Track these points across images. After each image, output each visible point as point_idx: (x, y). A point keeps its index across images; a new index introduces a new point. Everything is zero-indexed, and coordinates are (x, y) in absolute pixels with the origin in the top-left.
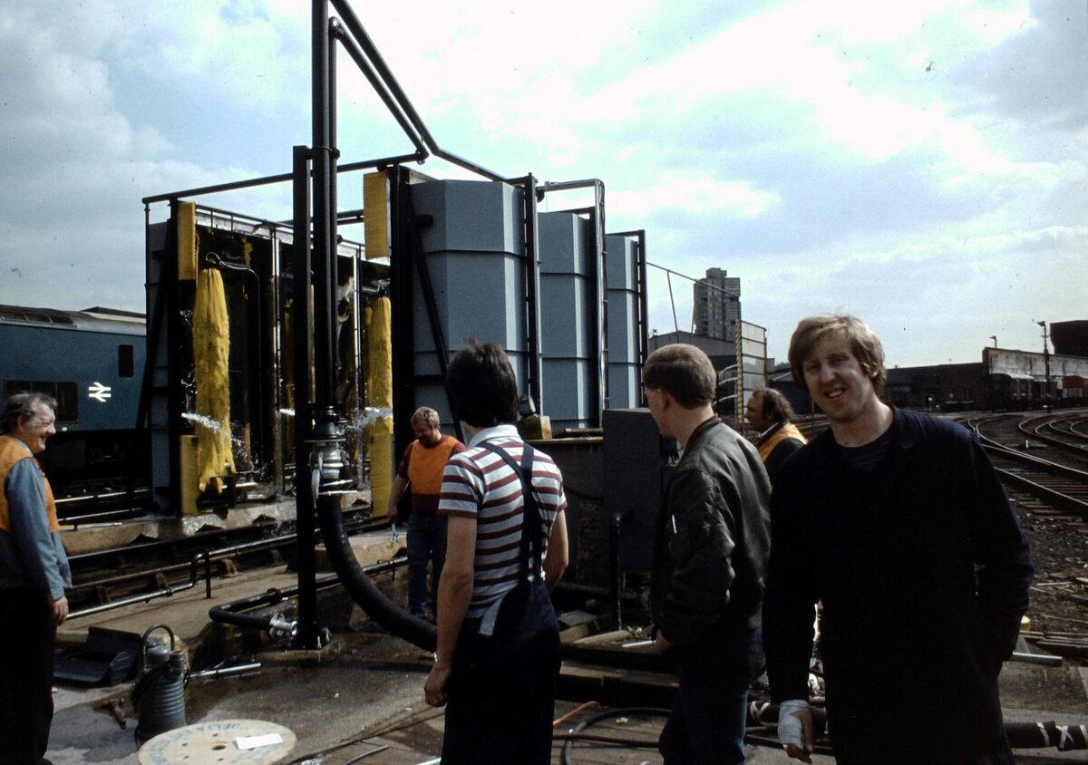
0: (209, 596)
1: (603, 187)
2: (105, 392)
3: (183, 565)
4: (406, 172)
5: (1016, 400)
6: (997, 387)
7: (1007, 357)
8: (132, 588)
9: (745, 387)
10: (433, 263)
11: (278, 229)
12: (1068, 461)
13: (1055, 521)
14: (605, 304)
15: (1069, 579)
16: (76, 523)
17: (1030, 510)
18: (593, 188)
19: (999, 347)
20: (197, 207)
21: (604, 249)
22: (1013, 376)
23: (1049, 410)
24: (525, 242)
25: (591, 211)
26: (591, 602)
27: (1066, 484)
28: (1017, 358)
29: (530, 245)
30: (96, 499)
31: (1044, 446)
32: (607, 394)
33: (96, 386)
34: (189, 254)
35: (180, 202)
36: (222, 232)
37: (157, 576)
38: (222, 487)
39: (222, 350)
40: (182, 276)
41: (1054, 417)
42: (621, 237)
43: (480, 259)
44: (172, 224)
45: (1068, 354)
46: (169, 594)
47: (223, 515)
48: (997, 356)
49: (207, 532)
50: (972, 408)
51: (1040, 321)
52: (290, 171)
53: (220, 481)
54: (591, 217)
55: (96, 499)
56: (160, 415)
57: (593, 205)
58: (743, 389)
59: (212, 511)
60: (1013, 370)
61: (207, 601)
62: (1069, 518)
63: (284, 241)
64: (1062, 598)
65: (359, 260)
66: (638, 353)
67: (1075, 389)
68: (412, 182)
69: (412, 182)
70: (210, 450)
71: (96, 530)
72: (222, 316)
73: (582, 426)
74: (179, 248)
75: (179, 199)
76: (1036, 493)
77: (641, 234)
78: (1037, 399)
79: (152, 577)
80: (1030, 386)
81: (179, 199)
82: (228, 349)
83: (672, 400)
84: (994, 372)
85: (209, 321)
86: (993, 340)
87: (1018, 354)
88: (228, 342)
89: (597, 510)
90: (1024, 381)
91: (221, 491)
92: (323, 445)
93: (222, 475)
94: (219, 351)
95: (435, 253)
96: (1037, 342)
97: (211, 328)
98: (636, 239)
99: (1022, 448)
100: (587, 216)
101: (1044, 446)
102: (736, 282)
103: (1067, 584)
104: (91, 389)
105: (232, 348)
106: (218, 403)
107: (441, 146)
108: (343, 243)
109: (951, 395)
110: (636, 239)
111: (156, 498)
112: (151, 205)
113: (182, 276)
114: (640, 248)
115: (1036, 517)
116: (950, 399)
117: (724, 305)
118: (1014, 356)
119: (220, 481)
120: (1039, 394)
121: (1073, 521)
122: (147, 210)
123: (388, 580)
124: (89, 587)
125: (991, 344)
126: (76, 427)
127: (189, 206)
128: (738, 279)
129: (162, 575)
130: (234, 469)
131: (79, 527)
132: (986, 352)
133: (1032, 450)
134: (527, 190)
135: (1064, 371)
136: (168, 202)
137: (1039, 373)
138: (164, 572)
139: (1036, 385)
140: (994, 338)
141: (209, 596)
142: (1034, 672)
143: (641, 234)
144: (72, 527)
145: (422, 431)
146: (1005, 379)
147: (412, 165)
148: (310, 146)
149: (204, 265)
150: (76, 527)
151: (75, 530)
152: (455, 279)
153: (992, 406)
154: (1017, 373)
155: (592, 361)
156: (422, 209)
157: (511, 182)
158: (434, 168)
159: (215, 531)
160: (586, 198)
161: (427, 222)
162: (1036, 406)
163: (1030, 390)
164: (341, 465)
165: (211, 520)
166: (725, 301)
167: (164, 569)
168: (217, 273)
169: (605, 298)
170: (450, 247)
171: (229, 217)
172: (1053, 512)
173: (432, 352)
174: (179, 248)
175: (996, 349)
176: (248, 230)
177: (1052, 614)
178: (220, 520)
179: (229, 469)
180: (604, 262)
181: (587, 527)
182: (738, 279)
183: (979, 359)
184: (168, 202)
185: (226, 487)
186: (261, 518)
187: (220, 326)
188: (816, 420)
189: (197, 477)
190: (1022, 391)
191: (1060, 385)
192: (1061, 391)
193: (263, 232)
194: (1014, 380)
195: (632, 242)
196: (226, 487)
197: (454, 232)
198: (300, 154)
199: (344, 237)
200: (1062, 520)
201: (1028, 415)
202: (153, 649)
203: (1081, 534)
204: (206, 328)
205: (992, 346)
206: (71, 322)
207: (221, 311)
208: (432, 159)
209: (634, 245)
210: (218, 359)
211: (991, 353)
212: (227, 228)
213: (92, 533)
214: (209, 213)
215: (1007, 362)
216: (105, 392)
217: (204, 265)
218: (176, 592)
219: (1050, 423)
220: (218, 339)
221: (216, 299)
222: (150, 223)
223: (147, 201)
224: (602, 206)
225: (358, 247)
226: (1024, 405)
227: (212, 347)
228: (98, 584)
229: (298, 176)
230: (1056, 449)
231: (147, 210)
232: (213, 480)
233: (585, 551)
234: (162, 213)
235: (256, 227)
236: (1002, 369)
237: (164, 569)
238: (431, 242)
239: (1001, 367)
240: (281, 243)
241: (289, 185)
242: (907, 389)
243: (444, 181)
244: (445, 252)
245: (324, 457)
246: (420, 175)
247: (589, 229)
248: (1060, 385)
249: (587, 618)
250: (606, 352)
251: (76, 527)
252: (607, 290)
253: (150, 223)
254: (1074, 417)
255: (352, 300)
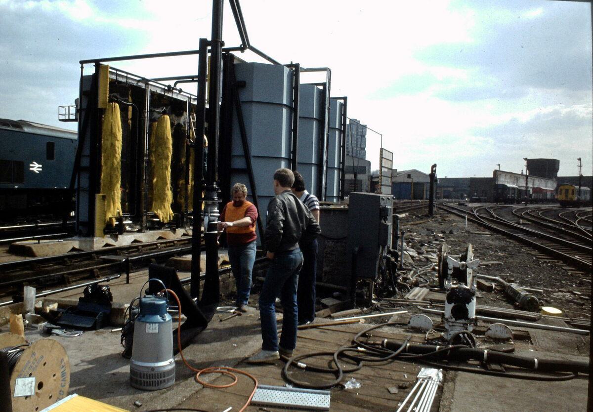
0: (128, 282)
1: (331, 72)
2: (33, 167)
3: (104, 265)
4: (232, 56)
5: (509, 198)
6: (500, 191)
7: (505, 176)
8: (80, 277)
9: (382, 184)
10: (245, 108)
11: (150, 83)
12: (539, 229)
13: (549, 262)
14: (328, 135)
15: (569, 292)
16: (39, 239)
17: (535, 256)
18: (326, 72)
19: (501, 170)
20: (111, 68)
21: (329, 105)
22: (508, 185)
23: (526, 204)
24: (294, 100)
25: (324, 84)
26: (335, 294)
27: (548, 243)
28: (511, 176)
29: (296, 101)
30: (37, 227)
31: (529, 223)
32: (326, 184)
33: (33, 164)
34: (104, 93)
35: (101, 64)
36: (121, 82)
37: (95, 270)
38: (115, 223)
39: (118, 148)
40: (100, 106)
41: (529, 208)
42: (335, 100)
43: (263, 106)
44: (95, 77)
45: (536, 175)
46: (108, 281)
47: (115, 238)
48: (500, 174)
49: (108, 248)
50: (486, 201)
51: (578, 158)
52: (197, 48)
53: (114, 220)
54: (323, 88)
55: (37, 227)
56: (85, 182)
57: (325, 81)
58: (381, 185)
59: (109, 236)
60: (508, 182)
61: (128, 285)
62: (556, 261)
63: (152, 90)
64: (569, 301)
65: (190, 103)
66: (339, 163)
67: (539, 194)
68: (235, 62)
69: (235, 62)
70: (109, 202)
71: (50, 243)
72: (119, 129)
73: (335, 200)
74: (103, 92)
75: (101, 63)
76: (535, 247)
77: (345, 99)
78: (520, 199)
79: (91, 271)
80: (516, 192)
81: (101, 63)
82: (121, 148)
83: (279, 184)
84: (498, 183)
85: (112, 132)
86: (498, 166)
87: (511, 174)
88: (121, 143)
89: (334, 244)
90: (513, 188)
91: (114, 225)
92: (210, 203)
93: (116, 216)
94: (117, 148)
95: (247, 102)
96: (521, 168)
97: (113, 135)
98: (342, 101)
99: (519, 223)
100: (321, 87)
101: (529, 223)
102: (364, 127)
103: (568, 294)
104: (31, 165)
105: (123, 146)
106: (115, 177)
107: (251, 44)
108: (182, 93)
109: (476, 194)
110: (342, 101)
111: (81, 228)
112: (84, 65)
113: (100, 106)
114: (344, 106)
115: (539, 259)
116: (474, 196)
117: (357, 139)
118: (509, 175)
119: (114, 220)
120: (521, 196)
121: (558, 262)
122: (82, 68)
123: (227, 278)
124: (60, 275)
125: (497, 168)
126: (23, 186)
127: (107, 67)
128: (200, 39)
129: (97, 270)
130: (121, 214)
131: (41, 241)
132: (495, 172)
133: (523, 224)
134: (295, 70)
135: (533, 184)
136: (94, 64)
137: (521, 185)
138: (98, 268)
139: (519, 191)
140: (499, 165)
141: (128, 282)
142: (577, 338)
143: (345, 99)
144: (37, 241)
145: (239, 197)
146: (504, 187)
147: (237, 54)
148: (209, 39)
149: (111, 100)
150: (39, 241)
151: (39, 243)
152: (256, 118)
153: (496, 200)
154: (510, 184)
155: (319, 166)
156: (240, 77)
157: (288, 66)
158: (248, 57)
159: (111, 247)
160: (321, 77)
161: (242, 85)
162: (518, 203)
163: (516, 193)
164: (219, 215)
165: (108, 240)
166: (359, 137)
167: (98, 266)
168: (117, 105)
169: (328, 132)
170: (254, 100)
171: (125, 75)
172: (546, 257)
173: (242, 156)
174: (103, 92)
175: (499, 171)
176: (135, 83)
177: (567, 309)
178: (114, 241)
179: (119, 213)
180: (329, 113)
181: (329, 253)
182: (200, 39)
183: (491, 176)
184: (94, 64)
185: (118, 223)
186: (135, 241)
187: (117, 134)
188: (413, 202)
189: (105, 213)
190: (512, 194)
191: (531, 192)
192: (531, 195)
193: (142, 85)
194: (509, 188)
195: (340, 103)
196: (118, 223)
197: (257, 91)
198: (203, 43)
199: (183, 91)
200: (552, 262)
201: (515, 206)
202: (134, 310)
203: (565, 270)
204: (109, 135)
205: (498, 169)
206: (22, 128)
207: (118, 127)
208: (247, 51)
209: (341, 105)
210: (116, 153)
211: (498, 173)
212: (124, 80)
213: (48, 245)
214: (115, 72)
215: (505, 179)
216: (33, 167)
217: (111, 100)
218: (112, 279)
219: (528, 211)
220: (117, 142)
221: (116, 122)
222: (84, 75)
223: (82, 62)
224: (330, 83)
225: (189, 96)
226: (512, 201)
227: (113, 146)
228: (65, 274)
229: (202, 52)
230: (536, 224)
231: (82, 68)
232: (111, 219)
233: (328, 266)
234: (90, 70)
235: (139, 81)
236: (503, 182)
237: (98, 266)
238: (244, 96)
239: (502, 181)
240: (150, 90)
241: (197, 56)
242: (451, 189)
243: (253, 64)
244: (252, 102)
245: (211, 209)
246: (239, 59)
247: (323, 94)
248: (531, 192)
249: (336, 302)
250: (327, 162)
251: (39, 241)
252: (329, 128)
253: (84, 75)
254: (539, 209)
255: (185, 125)
